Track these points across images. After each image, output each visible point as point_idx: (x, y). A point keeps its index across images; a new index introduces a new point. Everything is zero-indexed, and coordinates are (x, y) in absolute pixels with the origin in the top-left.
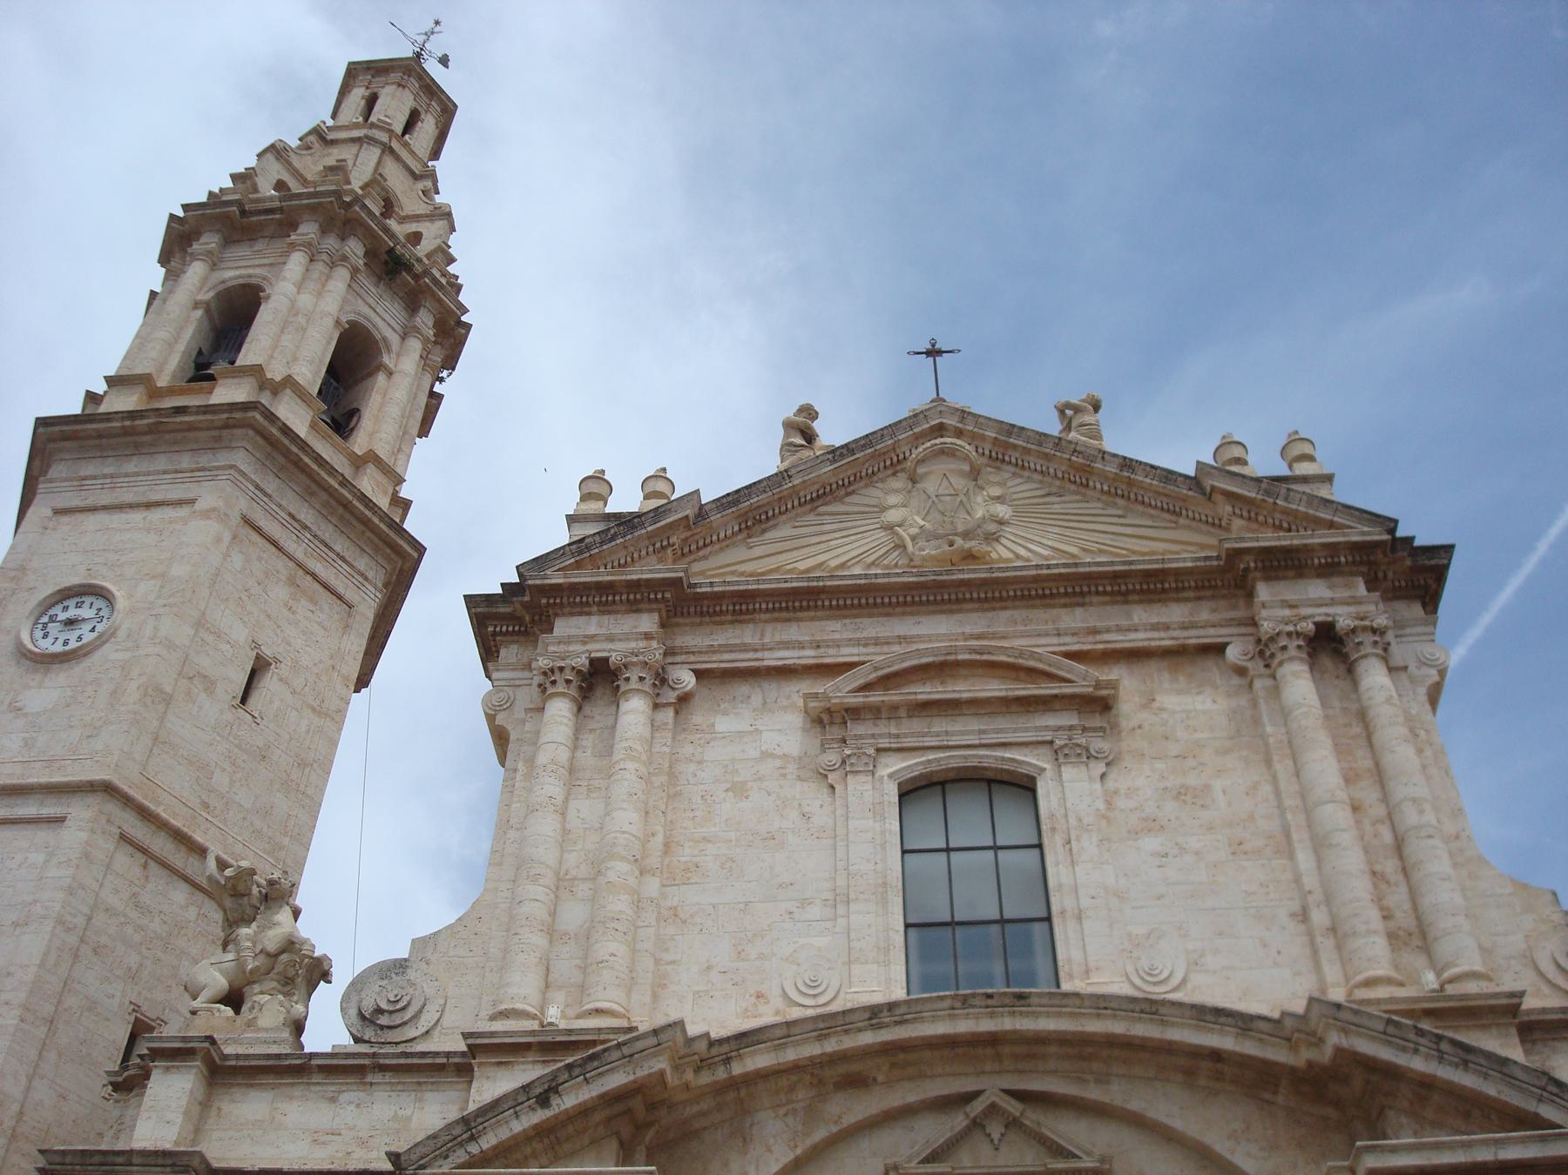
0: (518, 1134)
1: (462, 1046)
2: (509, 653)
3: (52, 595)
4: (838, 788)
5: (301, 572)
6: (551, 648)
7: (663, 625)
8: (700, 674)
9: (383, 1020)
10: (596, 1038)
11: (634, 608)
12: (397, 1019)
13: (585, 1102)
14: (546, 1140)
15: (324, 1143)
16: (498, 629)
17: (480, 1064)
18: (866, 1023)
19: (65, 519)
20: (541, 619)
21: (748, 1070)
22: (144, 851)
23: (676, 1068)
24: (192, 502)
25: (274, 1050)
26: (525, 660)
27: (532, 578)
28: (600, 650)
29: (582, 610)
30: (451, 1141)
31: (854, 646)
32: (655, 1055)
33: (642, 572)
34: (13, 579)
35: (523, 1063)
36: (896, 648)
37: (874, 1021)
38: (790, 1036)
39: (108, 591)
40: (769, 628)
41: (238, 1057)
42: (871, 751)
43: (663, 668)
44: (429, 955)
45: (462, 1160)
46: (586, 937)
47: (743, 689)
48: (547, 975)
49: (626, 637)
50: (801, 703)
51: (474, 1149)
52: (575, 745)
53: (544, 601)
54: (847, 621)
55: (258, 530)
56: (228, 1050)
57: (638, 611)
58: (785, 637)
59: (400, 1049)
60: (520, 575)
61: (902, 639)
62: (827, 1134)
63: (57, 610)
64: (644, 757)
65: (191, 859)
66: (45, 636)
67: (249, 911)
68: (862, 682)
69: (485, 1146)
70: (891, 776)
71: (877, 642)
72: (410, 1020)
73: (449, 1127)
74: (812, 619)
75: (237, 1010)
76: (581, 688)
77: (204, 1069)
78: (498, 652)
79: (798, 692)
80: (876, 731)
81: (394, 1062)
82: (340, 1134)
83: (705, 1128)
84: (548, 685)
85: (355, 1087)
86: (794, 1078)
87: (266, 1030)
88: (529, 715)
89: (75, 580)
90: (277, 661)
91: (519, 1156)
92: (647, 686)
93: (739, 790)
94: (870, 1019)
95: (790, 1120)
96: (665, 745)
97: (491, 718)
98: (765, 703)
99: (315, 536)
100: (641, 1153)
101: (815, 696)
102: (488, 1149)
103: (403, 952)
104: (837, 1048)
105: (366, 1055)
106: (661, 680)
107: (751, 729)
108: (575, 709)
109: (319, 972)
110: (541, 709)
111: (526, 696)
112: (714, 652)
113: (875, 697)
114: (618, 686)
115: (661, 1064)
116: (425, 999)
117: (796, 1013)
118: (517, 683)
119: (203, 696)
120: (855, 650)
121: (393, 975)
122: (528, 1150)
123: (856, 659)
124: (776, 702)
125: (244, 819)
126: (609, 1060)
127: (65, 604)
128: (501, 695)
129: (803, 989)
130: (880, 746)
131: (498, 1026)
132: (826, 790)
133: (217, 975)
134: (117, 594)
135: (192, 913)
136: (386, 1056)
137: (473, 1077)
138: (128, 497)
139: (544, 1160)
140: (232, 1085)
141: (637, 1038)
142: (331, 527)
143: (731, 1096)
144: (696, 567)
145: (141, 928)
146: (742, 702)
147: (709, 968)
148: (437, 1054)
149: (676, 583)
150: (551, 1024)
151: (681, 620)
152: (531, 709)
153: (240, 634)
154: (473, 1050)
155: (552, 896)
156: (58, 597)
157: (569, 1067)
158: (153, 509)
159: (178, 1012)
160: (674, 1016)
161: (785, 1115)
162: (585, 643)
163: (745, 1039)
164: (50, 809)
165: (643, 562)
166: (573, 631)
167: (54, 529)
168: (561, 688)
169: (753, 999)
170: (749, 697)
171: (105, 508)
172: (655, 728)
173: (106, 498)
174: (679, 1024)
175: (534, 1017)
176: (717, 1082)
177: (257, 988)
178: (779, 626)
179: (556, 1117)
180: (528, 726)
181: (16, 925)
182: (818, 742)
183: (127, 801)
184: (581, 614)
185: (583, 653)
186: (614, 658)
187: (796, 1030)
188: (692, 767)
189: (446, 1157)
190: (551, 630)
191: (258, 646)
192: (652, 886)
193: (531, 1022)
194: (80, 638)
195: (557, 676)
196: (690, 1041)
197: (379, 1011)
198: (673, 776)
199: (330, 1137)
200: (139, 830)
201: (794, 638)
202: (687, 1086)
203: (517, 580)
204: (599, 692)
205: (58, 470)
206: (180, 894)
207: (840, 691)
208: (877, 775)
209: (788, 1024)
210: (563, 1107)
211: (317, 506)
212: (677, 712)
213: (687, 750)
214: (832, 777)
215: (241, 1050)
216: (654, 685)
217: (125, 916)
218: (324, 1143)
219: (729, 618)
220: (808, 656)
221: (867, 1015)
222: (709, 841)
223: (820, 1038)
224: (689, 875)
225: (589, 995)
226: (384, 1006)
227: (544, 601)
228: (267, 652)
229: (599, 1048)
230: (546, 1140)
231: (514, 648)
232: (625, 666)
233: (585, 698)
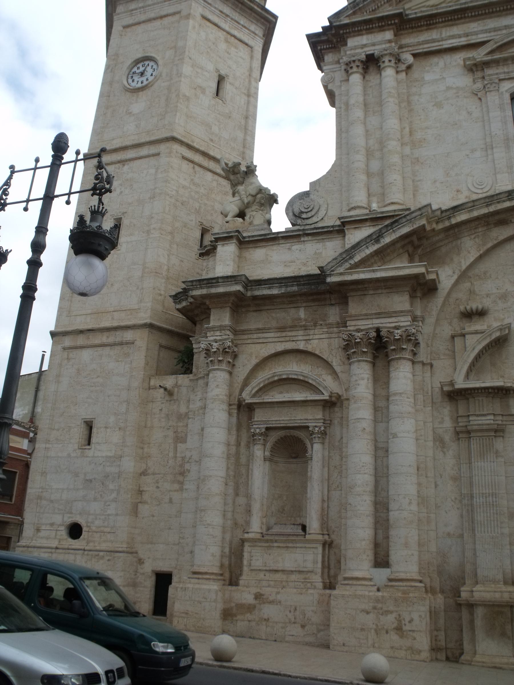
0: (369, 254)
1: (338, 223)
2: (329, 58)
3: (132, 63)
4: (483, 99)
5: (229, 36)
6: (348, 53)
7: (395, 35)
8: (415, 55)
9: (304, 216)
10: (394, 214)
11: (382, 29)
12: (309, 215)
13: (394, 240)
14: (379, 256)
15: (289, 266)
16: (322, 47)
17: (347, 229)
18: (506, 198)
19: (128, 30)
20: (340, 40)
21: (458, 221)
22: (192, 162)
23: (429, 222)
24: (179, 12)
25: (263, 232)
26: (336, 59)
27: (335, 22)
28: (370, 50)
29: (359, 33)
30: (342, 260)
31: (484, 33)
32: (420, 218)
33: (384, 12)
34: (114, 59)
35: (365, 227)
36: (504, 32)
37: (510, 197)
38: (474, 206)
39: (154, 58)
40: (444, 30)
41: (249, 237)
42: (497, 81)
43: (398, 55)
44: (317, 188)
45: (347, 267)
46: (382, 173)
47: (435, 60)
48: (368, 191)
49: (380, 43)
50: (462, 63)
51: (352, 262)
52: (365, 94)
53: (341, 32)
54: (480, 22)
55: (209, 20)
56: (245, 235)
57: (384, 30)
58: (452, 34)
59: (313, 226)
60: (330, 22)
61: (506, 27)
62: (492, 244)
63: (135, 69)
64: (396, 95)
65: (210, 163)
66: (133, 81)
67: (241, 179)
68: (490, 49)
69: (356, 260)
70: (506, 91)
71: (495, 30)
72: (315, 215)
73: (341, 254)
74: (463, 23)
75: (244, 219)
76: (363, 68)
77: (237, 243)
78: (323, 58)
79: (460, 58)
80: (498, 71)
81: (312, 231)
82: (295, 262)
83: (441, 246)
84: (349, 69)
85: (297, 243)
86: (477, 223)
87: (258, 225)
88: (342, 83)
89: (139, 55)
90: (227, 76)
91: (369, 263)
92: (392, 64)
93: (439, 105)
94: (508, 196)
95: (477, 240)
96: (404, 89)
97: (325, 87)
98: (445, 65)
99: (232, 19)
100: (417, 258)
101: (469, 59)
102: (357, 262)
103: (307, 188)
104: (495, 210)
105: (299, 230)
106: (399, 60)
107: (441, 77)
108: (362, 78)
109: (273, 199)
110: (348, 80)
111: (339, 75)
112: (420, 44)
113: (497, 56)
114: (380, 66)
115: (423, 222)
116: (320, 206)
117: (475, 197)
118: (335, 70)
119: (201, 95)
120: (485, 35)
121: (305, 198)
122: (373, 261)
123: (485, 39)
124: (450, 63)
125: (227, 143)
126: (402, 222)
127: (138, 66)
128: (329, 76)
129: (477, 186)
130: (501, 78)
131: (352, 213)
132: (478, 101)
133: (233, 206)
134: (158, 58)
135: (215, 184)
136: (307, 230)
137: (345, 234)
138: (152, 15)
139: (379, 264)
140: (249, 248)
141: (413, 212)
142: (237, 14)
143: (451, 232)
144: (407, 6)
145: (197, 192)
146: (435, 66)
147: (435, 181)
148: (328, 227)
149: (400, 15)
150: (374, 210)
151: (403, 32)
152: (343, 81)
153: (210, 67)
154: (344, 224)
155: (366, 159)
156: (134, 64)
157: (387, 226)
158: (164, 19)
159: (217, 223)
160: (425, 203)
161: (474, 238)
162: (362, 48)
163: (456, 209)
164: (153, 150)
165: (383, 7)
166: (356, 44)
167: (125, 35)
168: (355, 69)
169: (456, 193)
170: (438, 63)
171: (144, 22)
172: (399, 82)
173: (143, 18)
174: (429, 205)
175: (366, 209)
176: (445, 227)
177: (250, 210)
178: (448, 28)
179: (383, 246)
180: (343, 88)
181: (150, 198)
182: (471, 80)
183: (182, 143)
184: (359, 35)
185: (363, 52)
186: (376, 53)
187: (476, 203)
188: (417, 97)
189: (342, 266)
190: (346, 44)
191: (219, 71)
192: (407, 150)
193: (366, 210)
194: (147, 79)
195: (352, 65)
196: (433, 211)
197: (302, 212)
198: (409, 102)
199: (291, 264)
200: (189, 154)
201: (456, 33)
202: (433, 230)
203: (21, 375)
204: (371, 69)
205: (120, 9)
206: (209, 176)
207: (480, 55)
208: (500, 91)
209: (473, 201)
210: (385, 243)
211: (230, 5)
212: (407, 74)
213: (414, 90)
214: (479, 94)
215: (250, 234)
216: (396, 63)
217: (190, 188)
218: (289, 266)
219: (425, 28)
220: (463, 41)
221: (507, 195)
222: (428, 128)
223: (487, 206)
224: (422, 144)
225: (388, 197)
226: (303, 210)
227: (341, 32)
228: (223, 73)
229: (398, 218)
230: (379, 256)
231: (330, 55)
232: (382, 56)
233: (365, 72)
